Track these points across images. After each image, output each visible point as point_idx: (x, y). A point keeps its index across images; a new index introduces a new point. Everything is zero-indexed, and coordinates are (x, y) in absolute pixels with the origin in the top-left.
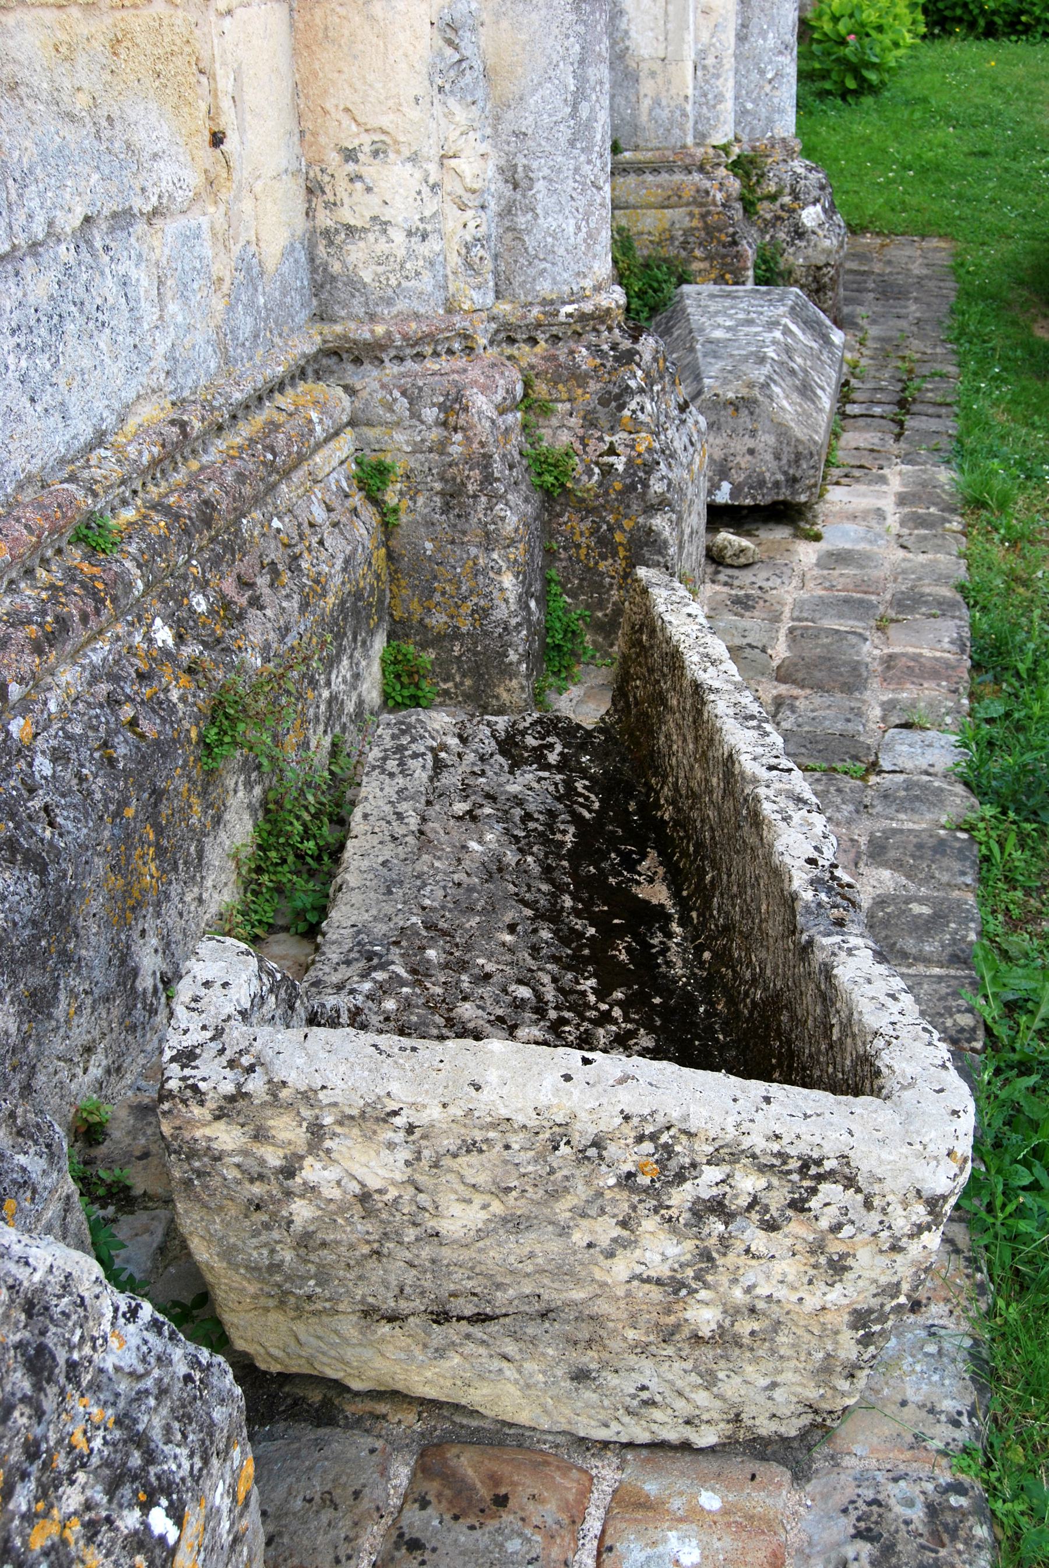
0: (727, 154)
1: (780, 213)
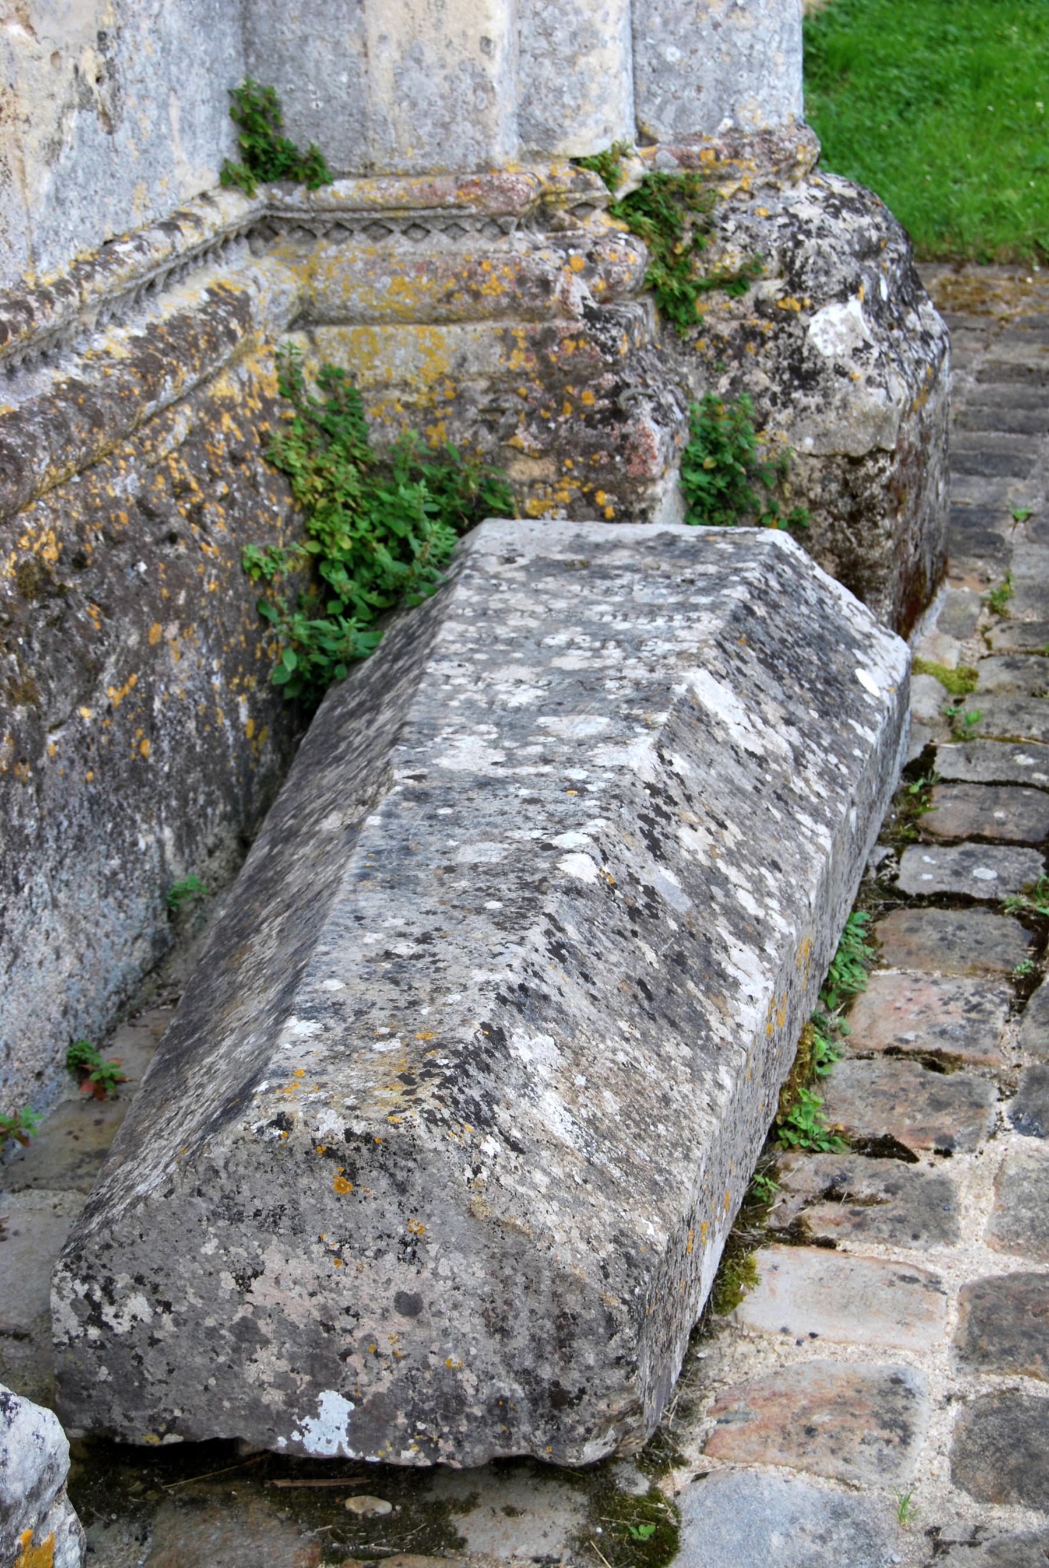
0: (610, 180)
1: (753, 320)
